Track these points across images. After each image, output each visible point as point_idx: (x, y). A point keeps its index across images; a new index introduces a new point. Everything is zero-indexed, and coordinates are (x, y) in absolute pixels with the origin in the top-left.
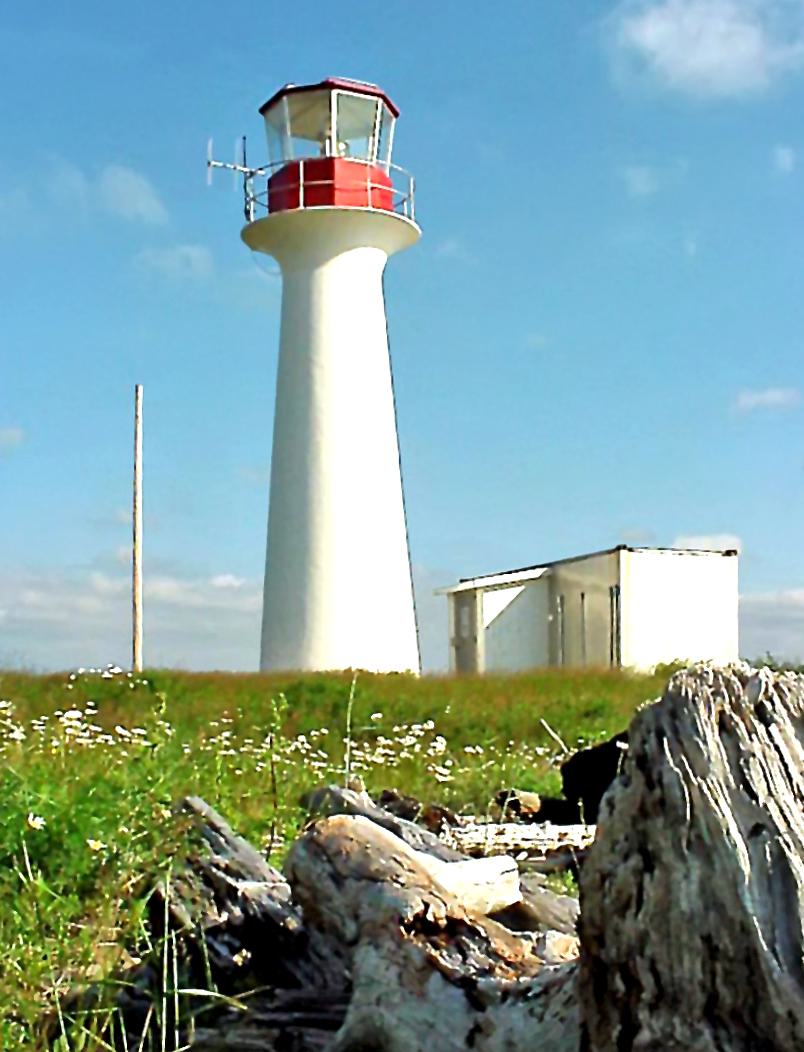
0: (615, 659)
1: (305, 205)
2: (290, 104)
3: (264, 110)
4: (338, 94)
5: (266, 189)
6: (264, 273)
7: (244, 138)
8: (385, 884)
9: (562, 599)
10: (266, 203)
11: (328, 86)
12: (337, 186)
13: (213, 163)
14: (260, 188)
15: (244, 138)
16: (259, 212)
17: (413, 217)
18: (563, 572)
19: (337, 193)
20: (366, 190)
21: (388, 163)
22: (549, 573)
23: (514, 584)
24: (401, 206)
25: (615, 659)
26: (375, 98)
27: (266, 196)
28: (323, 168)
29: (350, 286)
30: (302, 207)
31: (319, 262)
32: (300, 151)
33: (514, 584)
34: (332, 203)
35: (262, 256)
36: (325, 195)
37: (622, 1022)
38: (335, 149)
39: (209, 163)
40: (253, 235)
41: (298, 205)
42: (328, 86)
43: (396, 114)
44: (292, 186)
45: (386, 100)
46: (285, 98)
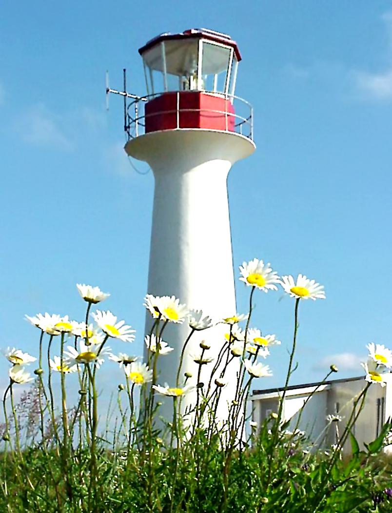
0: (220, 359)
1: (180, 127)
2: (166, 46)
3: (142, 51)
4: (204, 42)
5: (144, 115)
6: (140, 175)
7: (125, 70)
8: (29, 446)
9: (338, 405)
10: (144, 124)
11: (200, 36)
12: (201, 113)
13: (110, 90)
14: (139, 112)
15: (125, 70)
16: (139, 131)
17: (252, 139)
18: (339, 389)
19: (201, 118)
20: (225, 117)
21: (232, 94)
22: (328, 388)
23: (300, 396)
24: (239, 126)
25: (220, 359)
26: (229, 47)
27: (144, 119)
28: (192, 99)
29: (206, 186)
30: (178, 128)
31: (188, 170)
32: (165, 83)
33: (300, 396)
34: (199, 128)
35: (143, 165)
36: (192, 120)
37: (91, 455)
38: (197, 85)
39: (108, 91)
40: (133, 148)
41: (176, 127)
42: (191, 38)
43: (239, 59)
44: (174, 111)
45: (236, 50)
46: (163, 43)
